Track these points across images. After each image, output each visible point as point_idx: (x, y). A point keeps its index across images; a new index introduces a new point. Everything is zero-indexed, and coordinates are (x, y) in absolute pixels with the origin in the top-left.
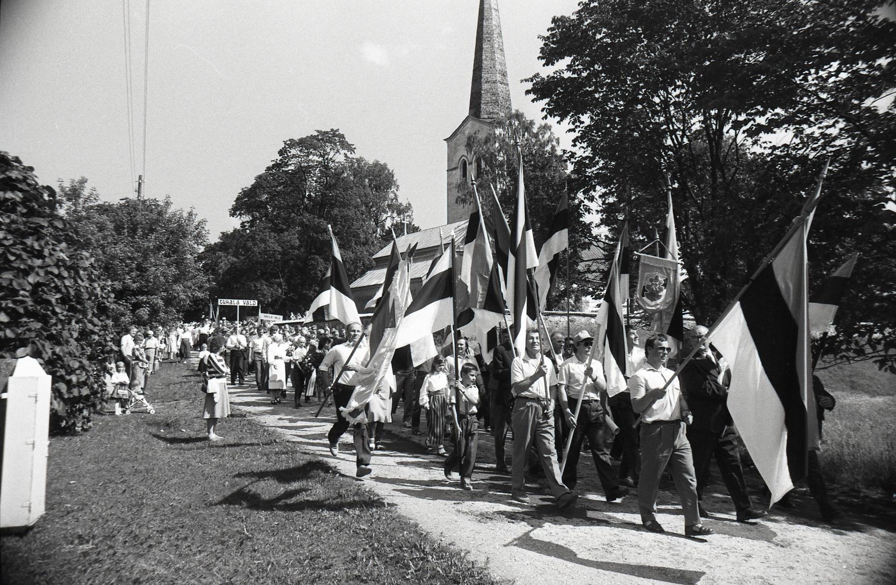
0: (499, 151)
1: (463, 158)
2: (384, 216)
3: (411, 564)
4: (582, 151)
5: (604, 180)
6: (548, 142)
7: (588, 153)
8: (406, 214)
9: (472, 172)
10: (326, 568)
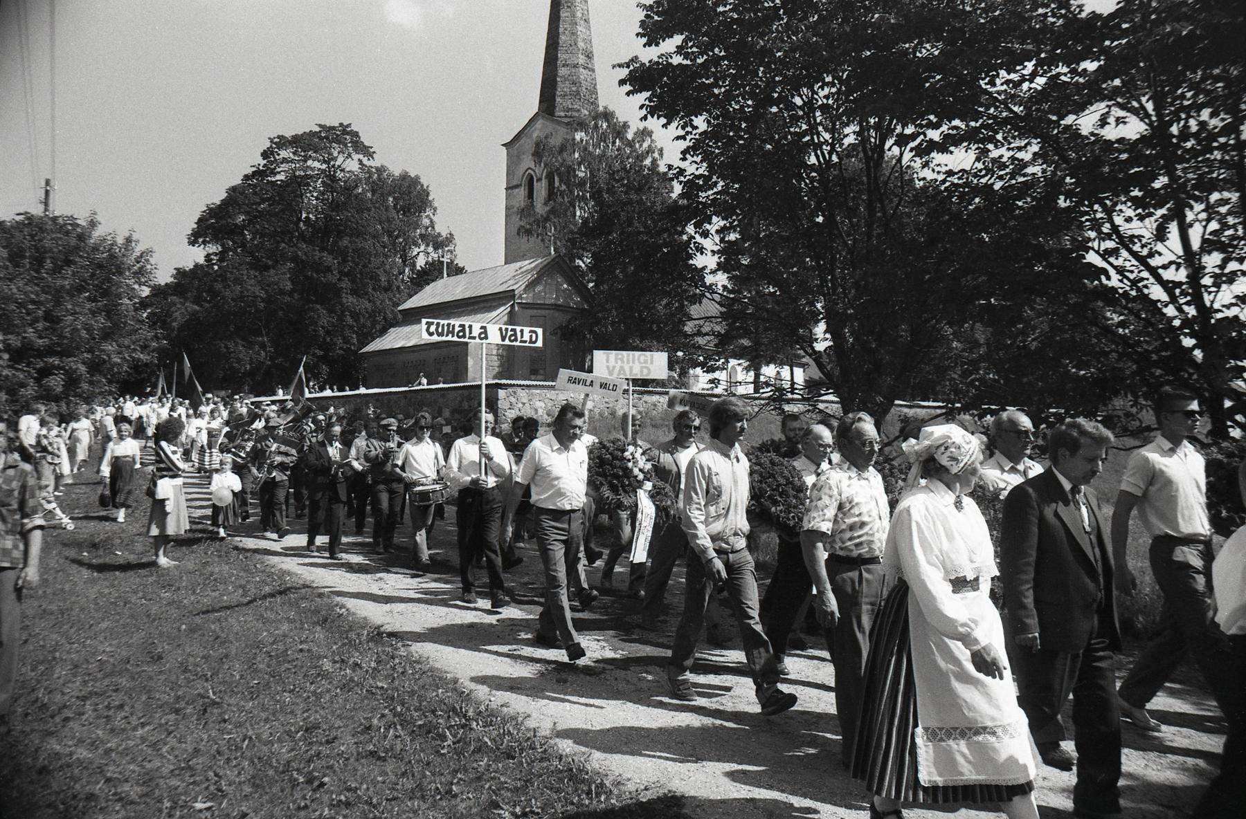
0: (579, 164)
1: (530, 171)
2: (416, 251)
3: (448, 734)
4: (695, 167)
6: (648, 153)
7: (703, 170)
9: (541, 190)
10: (328, 742)
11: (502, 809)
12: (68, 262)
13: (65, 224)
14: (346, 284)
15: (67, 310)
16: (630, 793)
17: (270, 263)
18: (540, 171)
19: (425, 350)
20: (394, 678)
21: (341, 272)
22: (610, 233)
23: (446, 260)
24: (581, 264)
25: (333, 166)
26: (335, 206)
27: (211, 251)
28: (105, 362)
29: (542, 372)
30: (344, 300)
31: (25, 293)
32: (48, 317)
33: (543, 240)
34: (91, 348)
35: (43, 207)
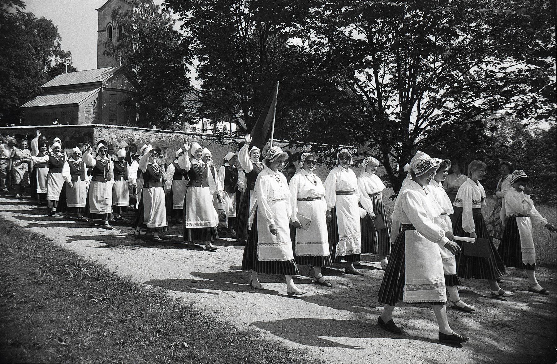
0: (135, 23)
1: (110, 24)
2: (50, 59)
3: (71, 273)
4: (186, 33)
5: (199, 52)
6: (168, 21)
7: (190, 34)
8: (67, 59)
9: (115, 34)
10: (14, 280)
11: (95, 298)
14: (11, 72)
16: (147, 289)
18: (114, 24)
19: (56, 108)
20: (45, 254)
21: (8, 66)
22: (149, 58)
23: (66, 64)
24: (135, 71)
29: (115, 121)
30: (11, 81)
33: (116, 58)
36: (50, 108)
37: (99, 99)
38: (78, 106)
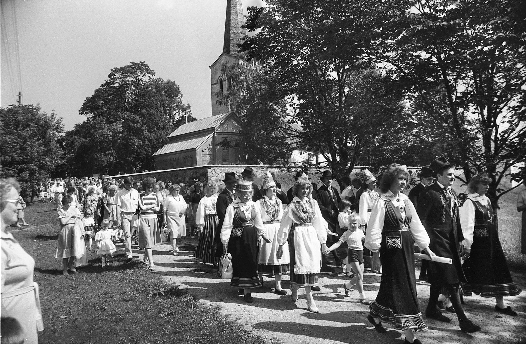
0: (241, 74)
2: (174, 112)
9: (226, 85)
10: (111, 297)
12: (28, 125)
13: (29, 109)
15: (29, 145)
17: (114, 120)
18: (224, 77)
21: (143, 123)
25: (138, 79)
26: (139, 96)
27: (89, 117)
28: (44, 165)
30: (145, 134)
31: (12, 139)
32: (21, 148)
33: (227, 106)
34: (39, 159)
35: (18, 103)
36: (174, 154)
37: (214, 143)
38: (196, 150)
